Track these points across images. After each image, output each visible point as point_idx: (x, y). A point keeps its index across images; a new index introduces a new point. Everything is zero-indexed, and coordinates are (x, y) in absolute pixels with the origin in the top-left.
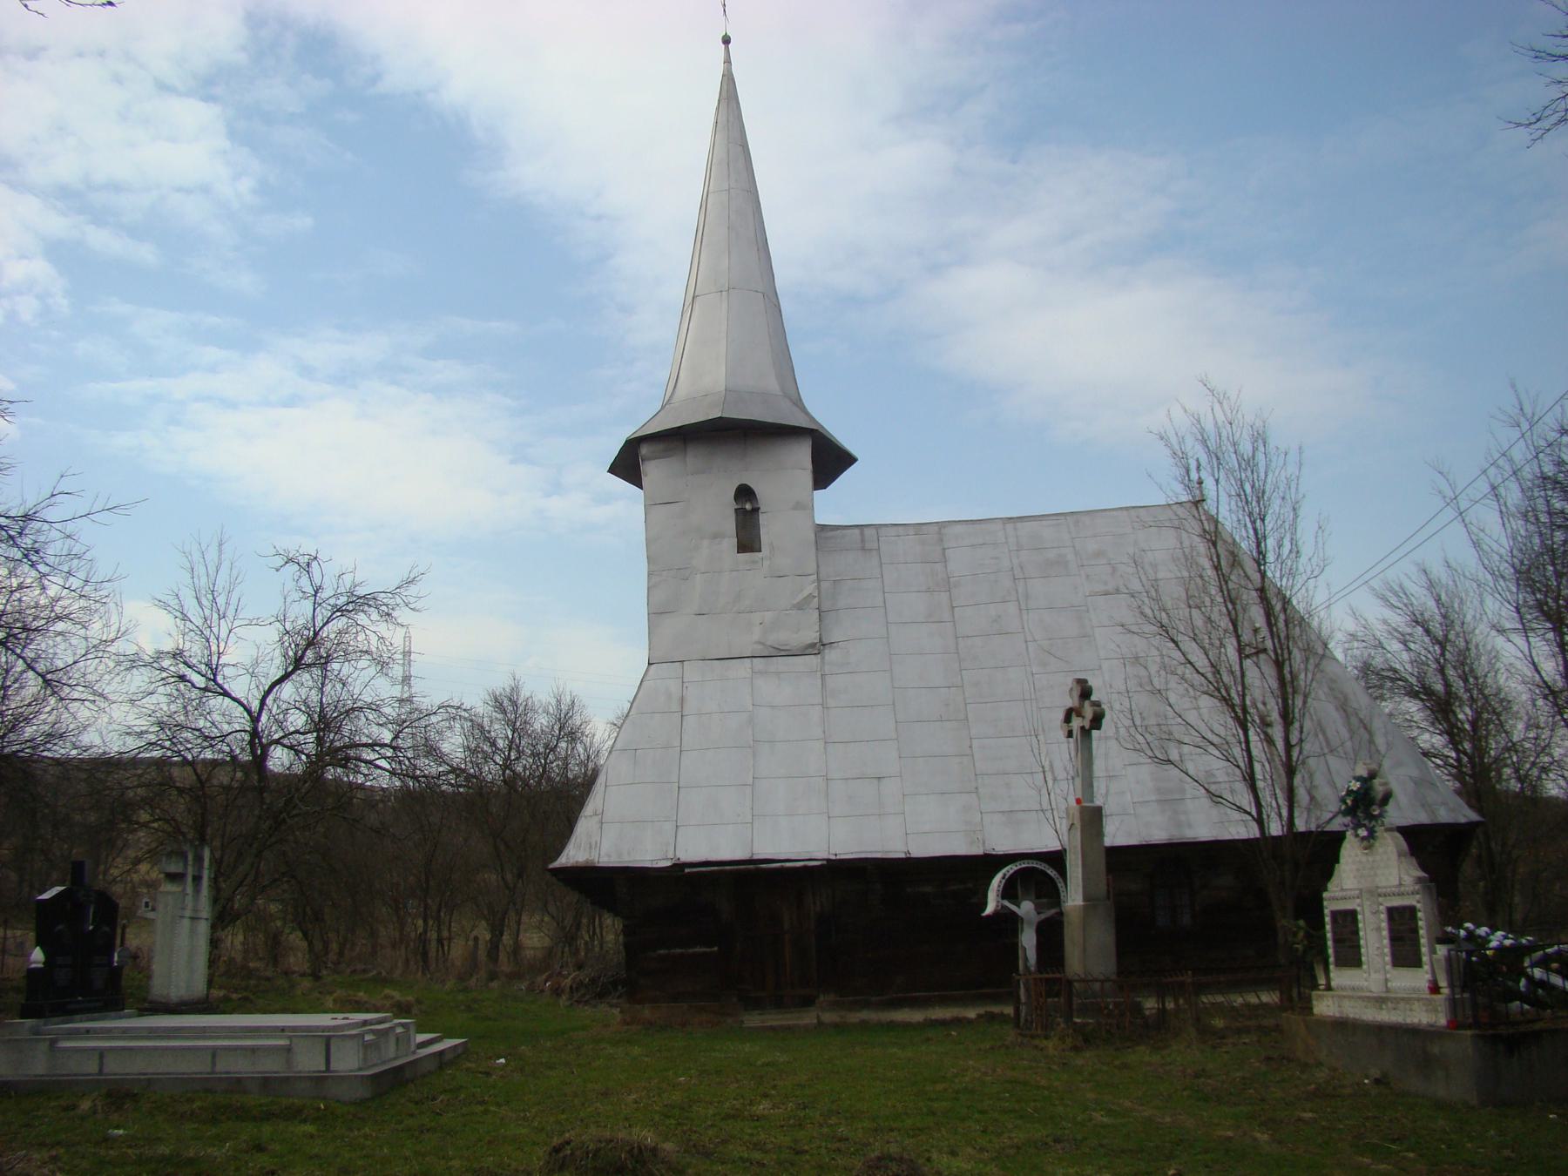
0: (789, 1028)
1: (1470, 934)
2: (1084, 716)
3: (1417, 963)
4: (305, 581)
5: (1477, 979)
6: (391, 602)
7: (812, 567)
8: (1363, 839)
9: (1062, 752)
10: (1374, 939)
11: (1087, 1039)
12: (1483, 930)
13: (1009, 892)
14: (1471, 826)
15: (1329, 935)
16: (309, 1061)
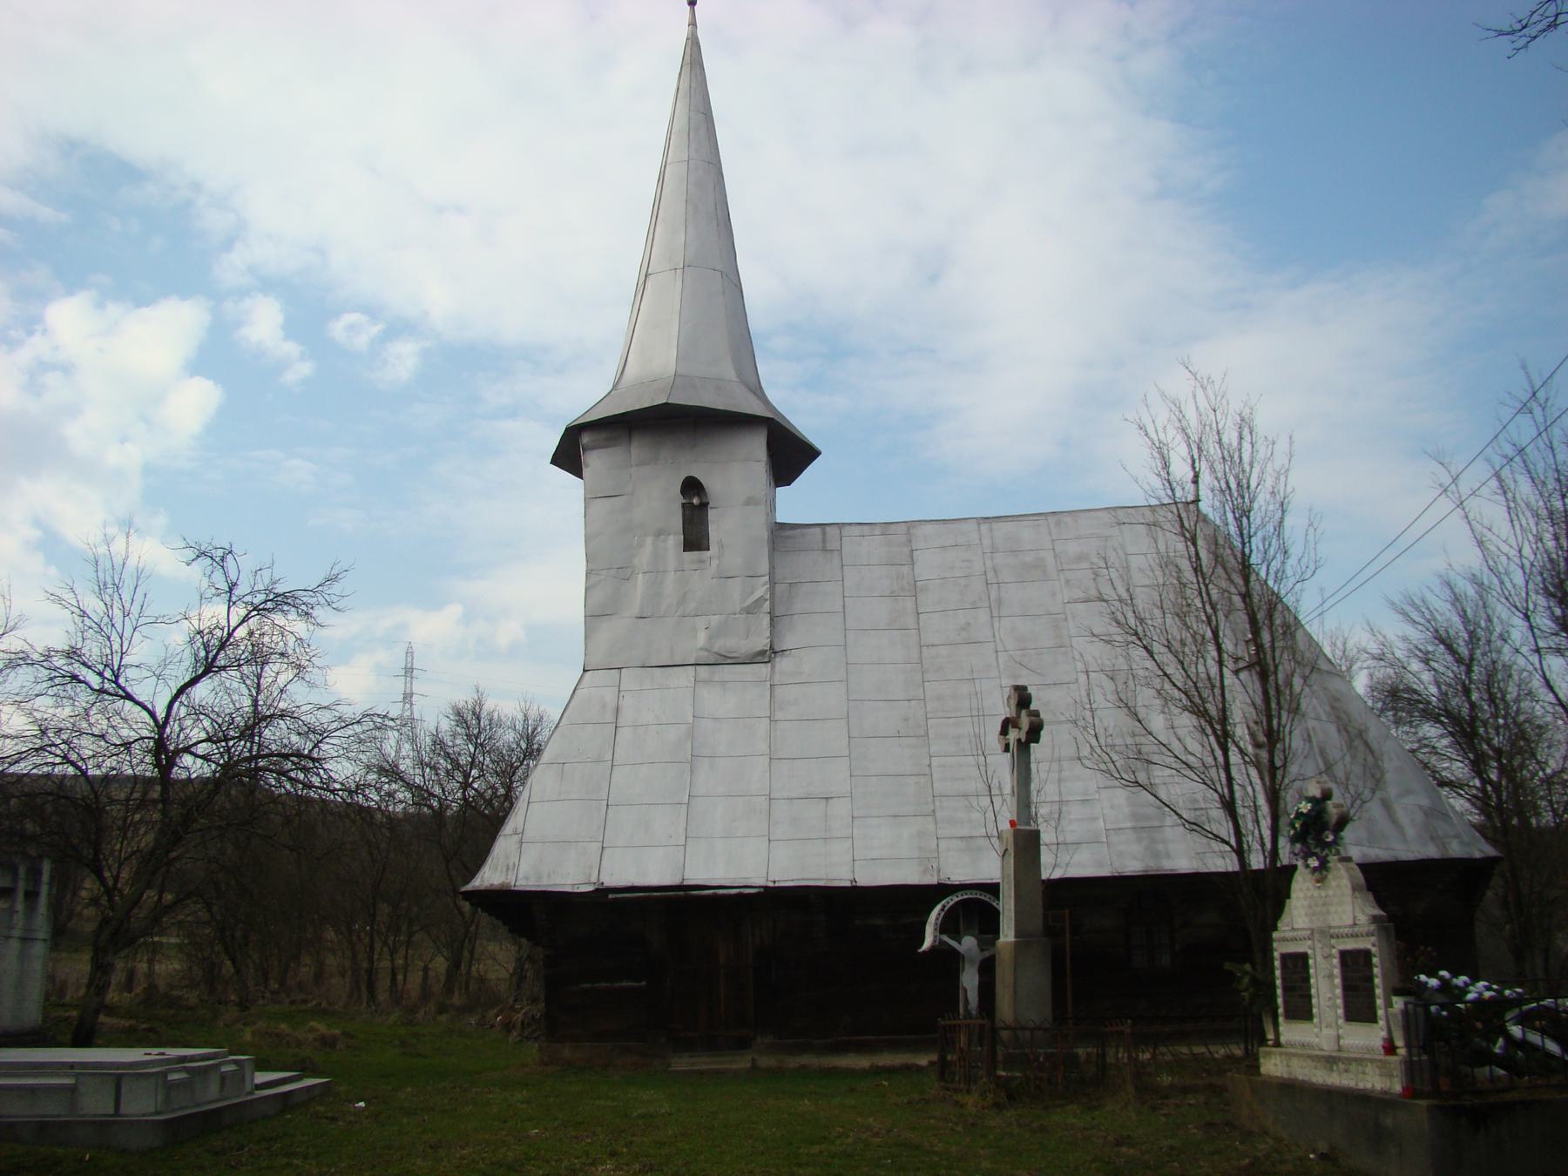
0: (718, 1072)
1: (1445, 984)
2: (1024, 726)
3: (1373, 1019)
4: (219, 578)
5: (1440, 1041)
6: (313, 601)
7: (764, 566)
8: (1315, 870)
9: (1002, 766)
10: (1326, 988)
11: (1011, 1095)
12: (1462, 980)
13: (949, 925)
14: (1488, 862)
15: (1278, 982)
16: (96, 1104)
